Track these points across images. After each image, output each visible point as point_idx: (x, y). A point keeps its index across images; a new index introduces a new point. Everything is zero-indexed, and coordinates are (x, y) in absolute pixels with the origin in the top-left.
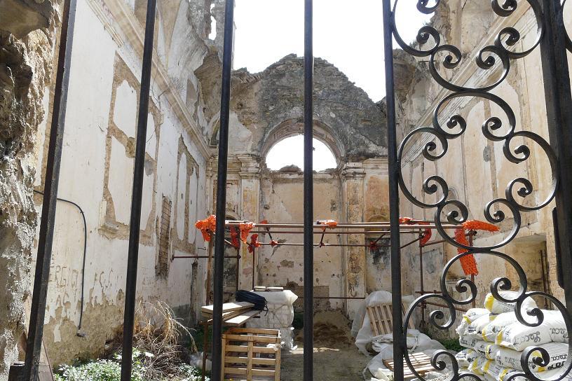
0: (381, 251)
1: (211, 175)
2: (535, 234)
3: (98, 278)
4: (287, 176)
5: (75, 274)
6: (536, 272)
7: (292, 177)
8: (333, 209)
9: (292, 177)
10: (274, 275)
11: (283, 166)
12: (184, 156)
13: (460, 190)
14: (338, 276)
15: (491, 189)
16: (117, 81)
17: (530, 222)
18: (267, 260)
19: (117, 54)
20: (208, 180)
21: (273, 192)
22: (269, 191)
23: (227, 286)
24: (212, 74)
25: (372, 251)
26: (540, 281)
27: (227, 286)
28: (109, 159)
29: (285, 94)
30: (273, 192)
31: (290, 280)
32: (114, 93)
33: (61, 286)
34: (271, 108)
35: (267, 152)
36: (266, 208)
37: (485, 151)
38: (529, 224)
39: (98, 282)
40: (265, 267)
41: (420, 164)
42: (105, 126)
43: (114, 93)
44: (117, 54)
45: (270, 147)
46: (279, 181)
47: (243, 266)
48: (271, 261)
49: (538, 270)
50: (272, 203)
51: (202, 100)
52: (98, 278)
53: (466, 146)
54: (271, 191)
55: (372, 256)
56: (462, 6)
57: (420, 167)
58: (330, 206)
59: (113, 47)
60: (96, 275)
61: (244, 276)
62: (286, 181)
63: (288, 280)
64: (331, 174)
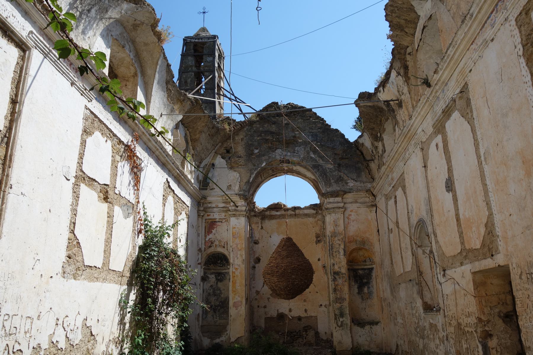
0: (365, 281)
1: (202, 214)
2: (499, 265)
3: (60, 322)
4: (274, 213)
5: (29, 321)
6: (507, 304)
7: (278, 213)
8: (318, 242)
9: (278, 213)
10: (265, 307)
11: (272, 203)
12: (170, 199)
13: (428, 221)
14: (325, 306)
15: (455, 220)
16: (87, 132)
17: (494, 253)
18: (258, 292)
19: (86, 108)
20: (200, 219)
21: (262, 228)
22: (258, 227)
23: (220, 319)
24: (199, 124)
25: (356, 281)
26: (512, 313)
27: (220, 319)
28: (77, 205)
29: (268, 138)
30: (262, 228)
31: (280, 311)
32: (83, 143)
33: (10, 335)
34: (256, 151)
35: (255, 191)
36: (256, 243)
37: (447, 183)
38: (492, 255)
39: (60, 327)
40: (256, 299)
41: (393, 197)
42: (73, 173)
43: (83, 143)
44: (86, 108)
45: (258, 186)
46: (267, 217)
47: (233, 299)
48: (261, 293)
49: (508, 302)
50: (260, 238)
51: (191, 147)
52: (60, 322)
53: (429, 179)
54: (260, 227)
55: (356, 286)
56: (416, 48)
57: (393, 200)
58: (315, 239)
59: (84, 101)
60: (58, 319)
61: (234, 308)
62: (272, 217)
63: (278, 310)
64: (314, 209)
